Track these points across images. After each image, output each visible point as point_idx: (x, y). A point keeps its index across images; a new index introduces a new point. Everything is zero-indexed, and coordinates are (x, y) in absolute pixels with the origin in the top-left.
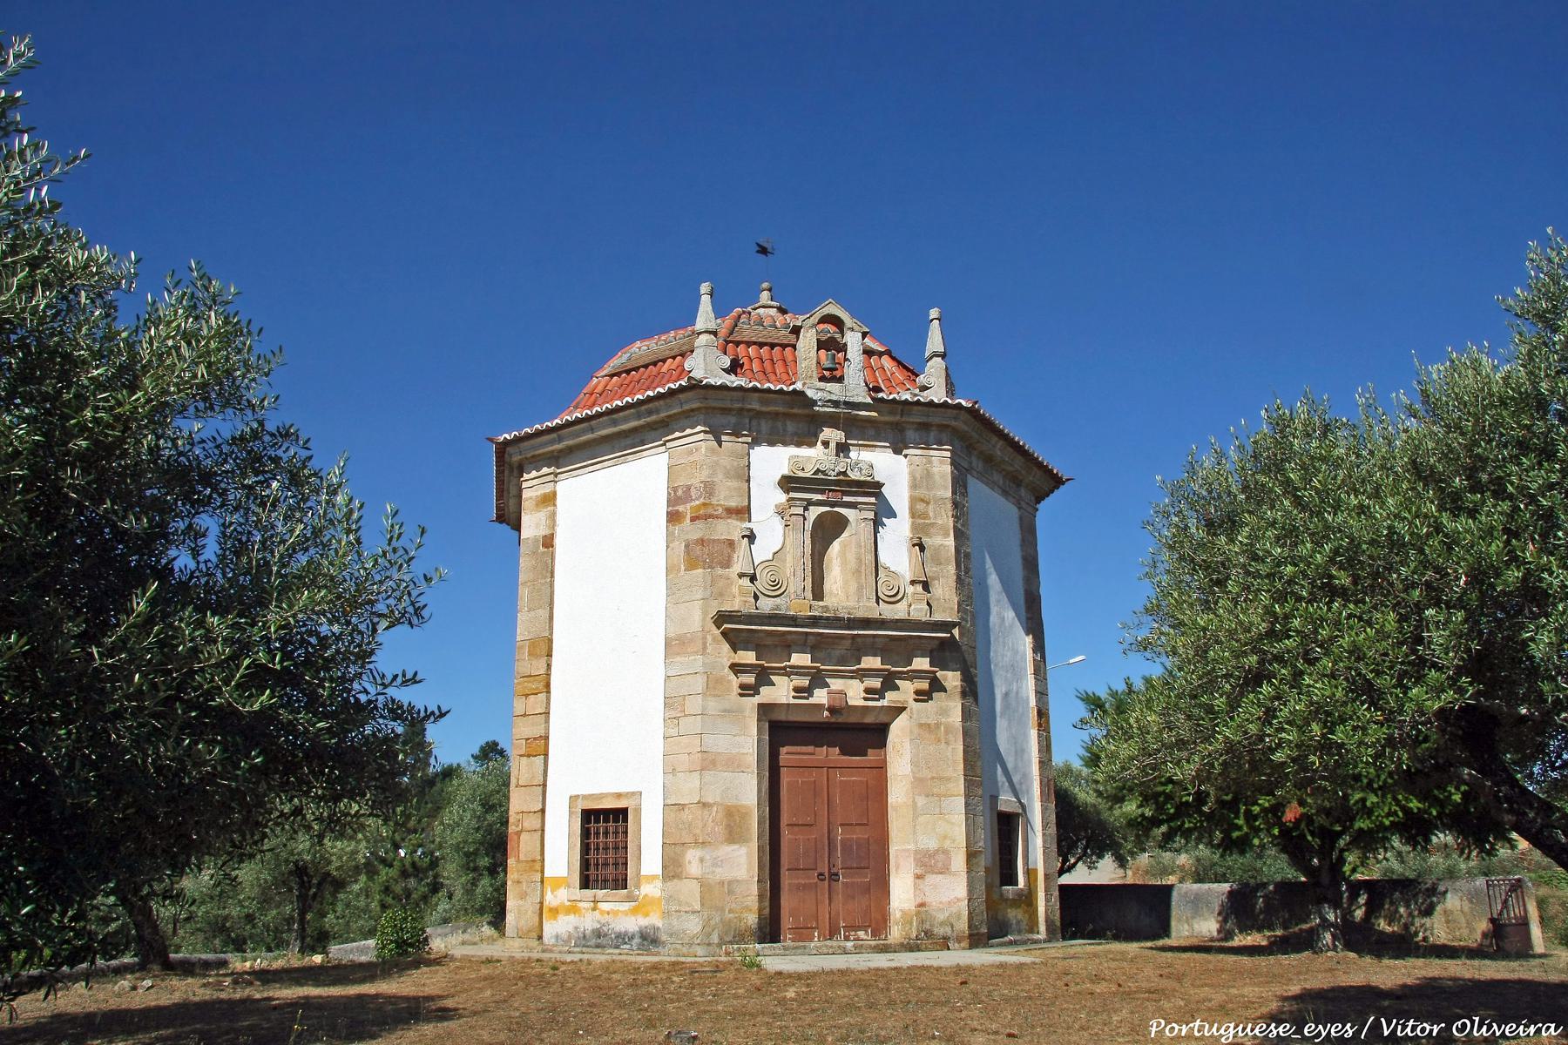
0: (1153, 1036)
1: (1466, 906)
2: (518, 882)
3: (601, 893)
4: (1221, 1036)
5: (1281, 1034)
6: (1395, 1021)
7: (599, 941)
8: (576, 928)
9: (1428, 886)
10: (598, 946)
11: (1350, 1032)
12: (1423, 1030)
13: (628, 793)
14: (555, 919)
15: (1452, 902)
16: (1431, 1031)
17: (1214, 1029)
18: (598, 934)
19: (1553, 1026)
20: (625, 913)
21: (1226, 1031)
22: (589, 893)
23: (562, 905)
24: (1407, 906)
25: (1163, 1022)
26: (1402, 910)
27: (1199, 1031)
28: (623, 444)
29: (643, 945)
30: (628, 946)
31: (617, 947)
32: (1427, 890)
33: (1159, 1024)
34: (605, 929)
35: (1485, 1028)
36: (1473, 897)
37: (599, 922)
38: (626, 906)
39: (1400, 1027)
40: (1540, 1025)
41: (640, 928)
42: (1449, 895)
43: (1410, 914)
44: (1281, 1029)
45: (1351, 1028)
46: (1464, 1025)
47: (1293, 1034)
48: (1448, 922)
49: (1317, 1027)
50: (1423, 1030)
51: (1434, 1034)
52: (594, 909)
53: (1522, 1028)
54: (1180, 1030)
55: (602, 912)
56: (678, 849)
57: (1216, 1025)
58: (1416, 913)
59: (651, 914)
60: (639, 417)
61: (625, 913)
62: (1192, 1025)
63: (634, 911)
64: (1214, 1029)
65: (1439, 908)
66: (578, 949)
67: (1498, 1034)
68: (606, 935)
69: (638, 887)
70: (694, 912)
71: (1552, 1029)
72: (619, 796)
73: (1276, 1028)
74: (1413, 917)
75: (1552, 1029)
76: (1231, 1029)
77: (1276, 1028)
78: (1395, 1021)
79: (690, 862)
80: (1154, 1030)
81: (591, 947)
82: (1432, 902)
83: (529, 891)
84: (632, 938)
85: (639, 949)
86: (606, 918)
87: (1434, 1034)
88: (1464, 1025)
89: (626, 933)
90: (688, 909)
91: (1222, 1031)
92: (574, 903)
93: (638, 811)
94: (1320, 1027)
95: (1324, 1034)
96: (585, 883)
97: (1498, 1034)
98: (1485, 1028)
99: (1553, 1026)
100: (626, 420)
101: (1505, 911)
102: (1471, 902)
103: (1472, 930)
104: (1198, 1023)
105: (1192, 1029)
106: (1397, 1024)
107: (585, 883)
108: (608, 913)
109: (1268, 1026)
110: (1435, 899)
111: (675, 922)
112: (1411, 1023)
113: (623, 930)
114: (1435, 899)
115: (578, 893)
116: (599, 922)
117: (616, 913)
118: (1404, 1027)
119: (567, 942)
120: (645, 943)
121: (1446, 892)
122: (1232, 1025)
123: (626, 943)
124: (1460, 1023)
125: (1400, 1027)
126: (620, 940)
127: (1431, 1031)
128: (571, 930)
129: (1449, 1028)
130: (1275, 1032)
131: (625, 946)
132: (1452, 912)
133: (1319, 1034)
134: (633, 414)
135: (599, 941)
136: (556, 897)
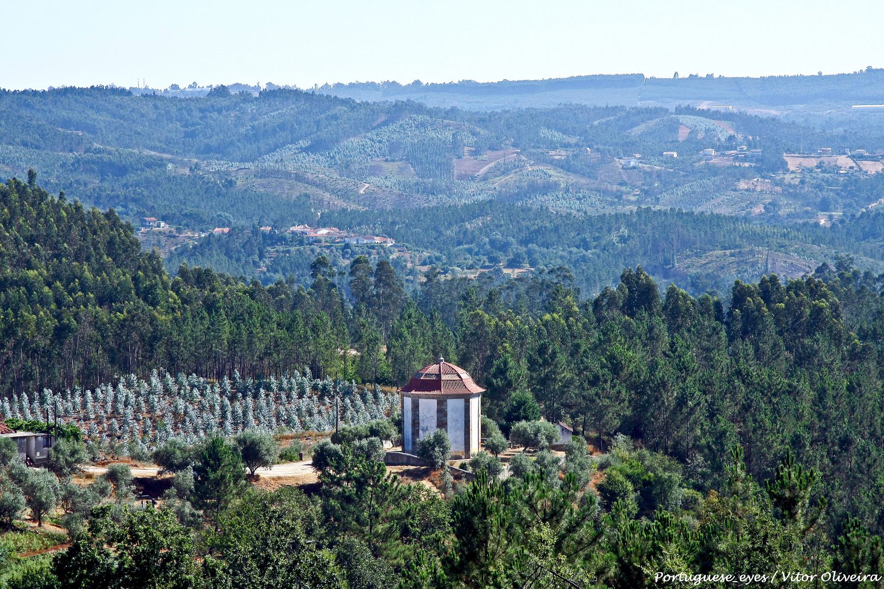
11: (765, 579)
12: (805, 578)
44: (727, 578)
53: (859, 577)
54: (809, 579)
71: (876, 578)
75: (876, 578)
76: (700, 577)
94: (749, 576)
95: (750, 580)
97: (846, 580)
98: (839, 577)
99: (876, 576)
105: (678, 577)
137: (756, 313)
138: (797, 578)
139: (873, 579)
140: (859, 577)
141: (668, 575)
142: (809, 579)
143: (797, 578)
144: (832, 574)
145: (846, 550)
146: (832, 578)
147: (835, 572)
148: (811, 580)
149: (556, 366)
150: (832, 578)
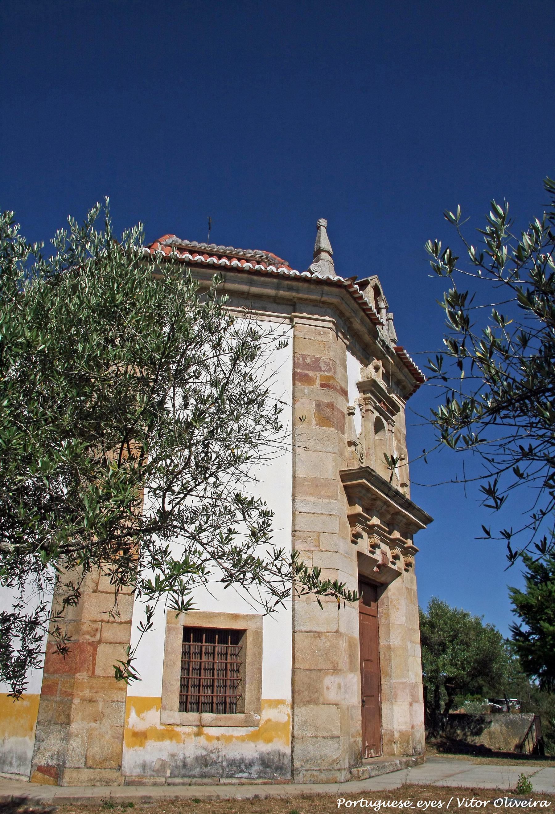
0: (339, 807)
1: (504, 729)
2: (90, 701)
3: (208, 716)
4: (374, 807)
5: (405, 806)
6: (464, 799)
7: (205, 770)
8: (173, 756)
9: (477, 718)
10: (203, 776)
11: (441, 805)
12: (479, 804)
13: (247, 615)
14: (142, 744)
15: (495, 727)
16: (483, 804)
17: (371, 804)
18: (203, 761)
19: (546, 802)
20: (242, 739)
21: (377, 804)
22: (193, 716)
23: (153, 729)
24: (463, 729)
25: (344, 800)
26: (459, 732)
27: (363, 805)
28: (257, 305)
29: (265, 773)
30: (245, 775)
31: (231, 776)
32: (478, 720)
33: (342, 801)
34: (214, 756)
35: (511, 803)
36: (511, 724)
37: (205, 749)
38: (242, 732)
39: (467, 802)
40: (539, 801)
41: (261, 754)
42: (493, 724)
43: (465, 734)
44: (405, 804)
45: (442, 803)
46: (500, 802)
47: (411, 806)
48: (490, 738)
49: (424, 803)
50: (479, 804)
51: (485, 806)
52: (198, 734)
53: (530, 803)
54: (353, 804)
55: (209, 738)
56: (314, 675)
57: (371, 802)
58: (469, 733)
59: (275, 740)
60: (278, 287)
61: (242, 739)
62: (359, 801)
63: (254, 737)
64: (371, 804)
65: (485, 731)
66: (178, 780)
67: (517, 806)
68: (214, 763)
69: (258, 710)
70: (333, 737)
71: (545, 804)
72: (235, 617)
73: (403, 803)
74: (467, 736)
75: (545, 804)
76: (379, 804)
77: (403, 803)
78: (464, 799)
79: (328, 688)
80: (339, 804)
81: (194, 776)
82: (482, 727)
83: (107, 711)
84: (251, 764)
85: (260, 777)
86: (216, 744)
87: (485, 806)
88: (500, 802)
89: (242, 760)
90: (326, 734)
91: (375, 805)
92: (170, 728)
93: (259, 634)
94: (426, 802)
95: (427, 806)
96: (184, 706)
97: (517, 806)
98: (511, 803)
99: (546, 802)
100: (264, 285)
101: (530, 733)
102: (508, 727)
103: (507, 743)
104: (362, 800)
105: (359, 803)
106: (465, 801)
107: (184, 706)
108: (218, 739)
109: (399, 802)
110: (483, 726)
111: (311, 748)
112: (472, 800)
113: (238, 757)
114: (483, 726)
115: (177, 716)
116: (205, 749)
117: (229, 739)
118: (469, 803)
119: (160, 771)
120: (268, 770)
121: (491, 722)
122: (380, 801)
123: (242, 771)
124: (497, 800)
125: (467, 802)
126: (234, 768)
127: (483, 804)
128: (165, 757)
129: (492, 803)
130: (402, 805)
131: (241, 775)
132: (494, 733)
133: (425, 805)
134: (274, 283)
135: (205, 770)
136: (143, 719)
137: (396, 535)
138: (471, 804)
139: (543, 804)
140: (530, 803)
141: (350, 801)
142: (353, 804)
143: (471, 804)
144: (504, 800)
145: (212, 770)
146: (504, 803)
147: (507, 798)
148: (354, 806)
149: (236, 460)
150: (504, 803)
